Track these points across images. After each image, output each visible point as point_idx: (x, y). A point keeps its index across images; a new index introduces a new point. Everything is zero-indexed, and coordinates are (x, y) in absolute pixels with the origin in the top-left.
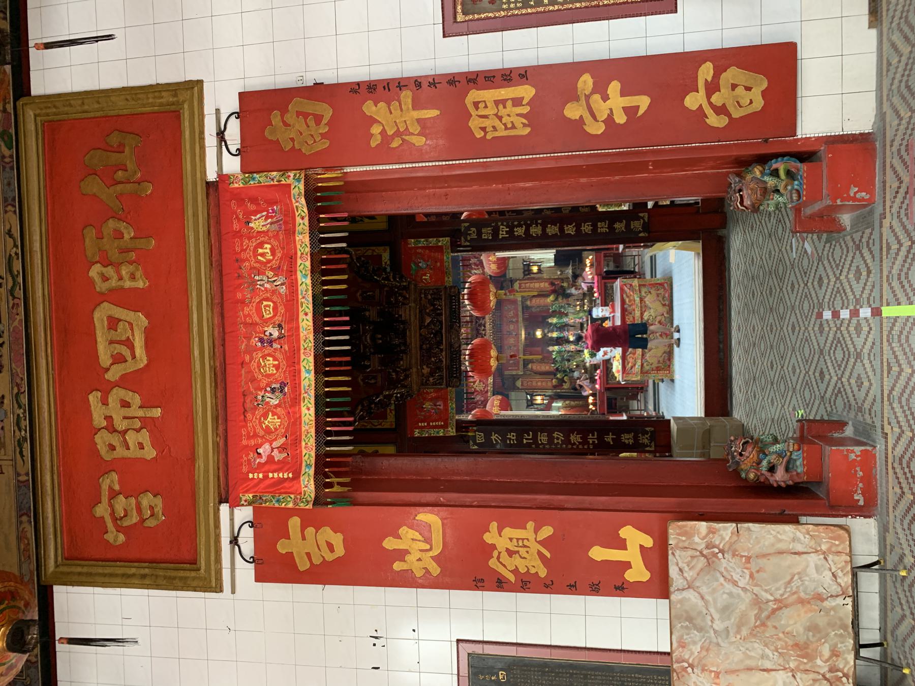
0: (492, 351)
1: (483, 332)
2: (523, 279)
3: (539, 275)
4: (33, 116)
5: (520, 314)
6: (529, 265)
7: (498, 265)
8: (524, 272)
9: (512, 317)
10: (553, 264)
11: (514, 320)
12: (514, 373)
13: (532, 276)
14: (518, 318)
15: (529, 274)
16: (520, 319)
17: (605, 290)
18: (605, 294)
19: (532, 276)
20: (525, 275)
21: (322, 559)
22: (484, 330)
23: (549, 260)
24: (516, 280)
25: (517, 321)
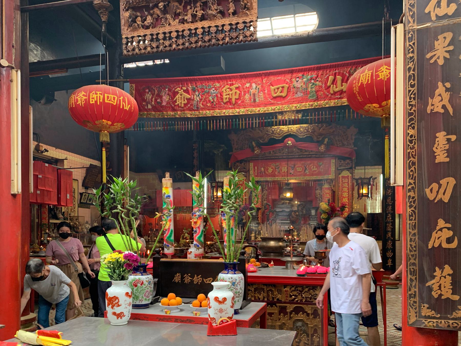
0: (363, 223)
1: (189, 17)
2: (353, 178)
3: (356, 195)
4: (337, 332)
5: (314, 178)
6: (369, 184)
7: (370, 86)
8: (361, 179)
9: (310, 169)
10: (369, 212)
11: (307, 171)
12: (251, 172)
13: (356, 188)
14: (309, 175)
15: (358, 184)
16: (308, 178)
17: (307, 286)
18: (302, 286)
19: (356, 188)
20: (357, 180)
21: (451, 290)
22: (194, 16)
23: (374, 207)
24: (352, 173)
25: (305, 175)
